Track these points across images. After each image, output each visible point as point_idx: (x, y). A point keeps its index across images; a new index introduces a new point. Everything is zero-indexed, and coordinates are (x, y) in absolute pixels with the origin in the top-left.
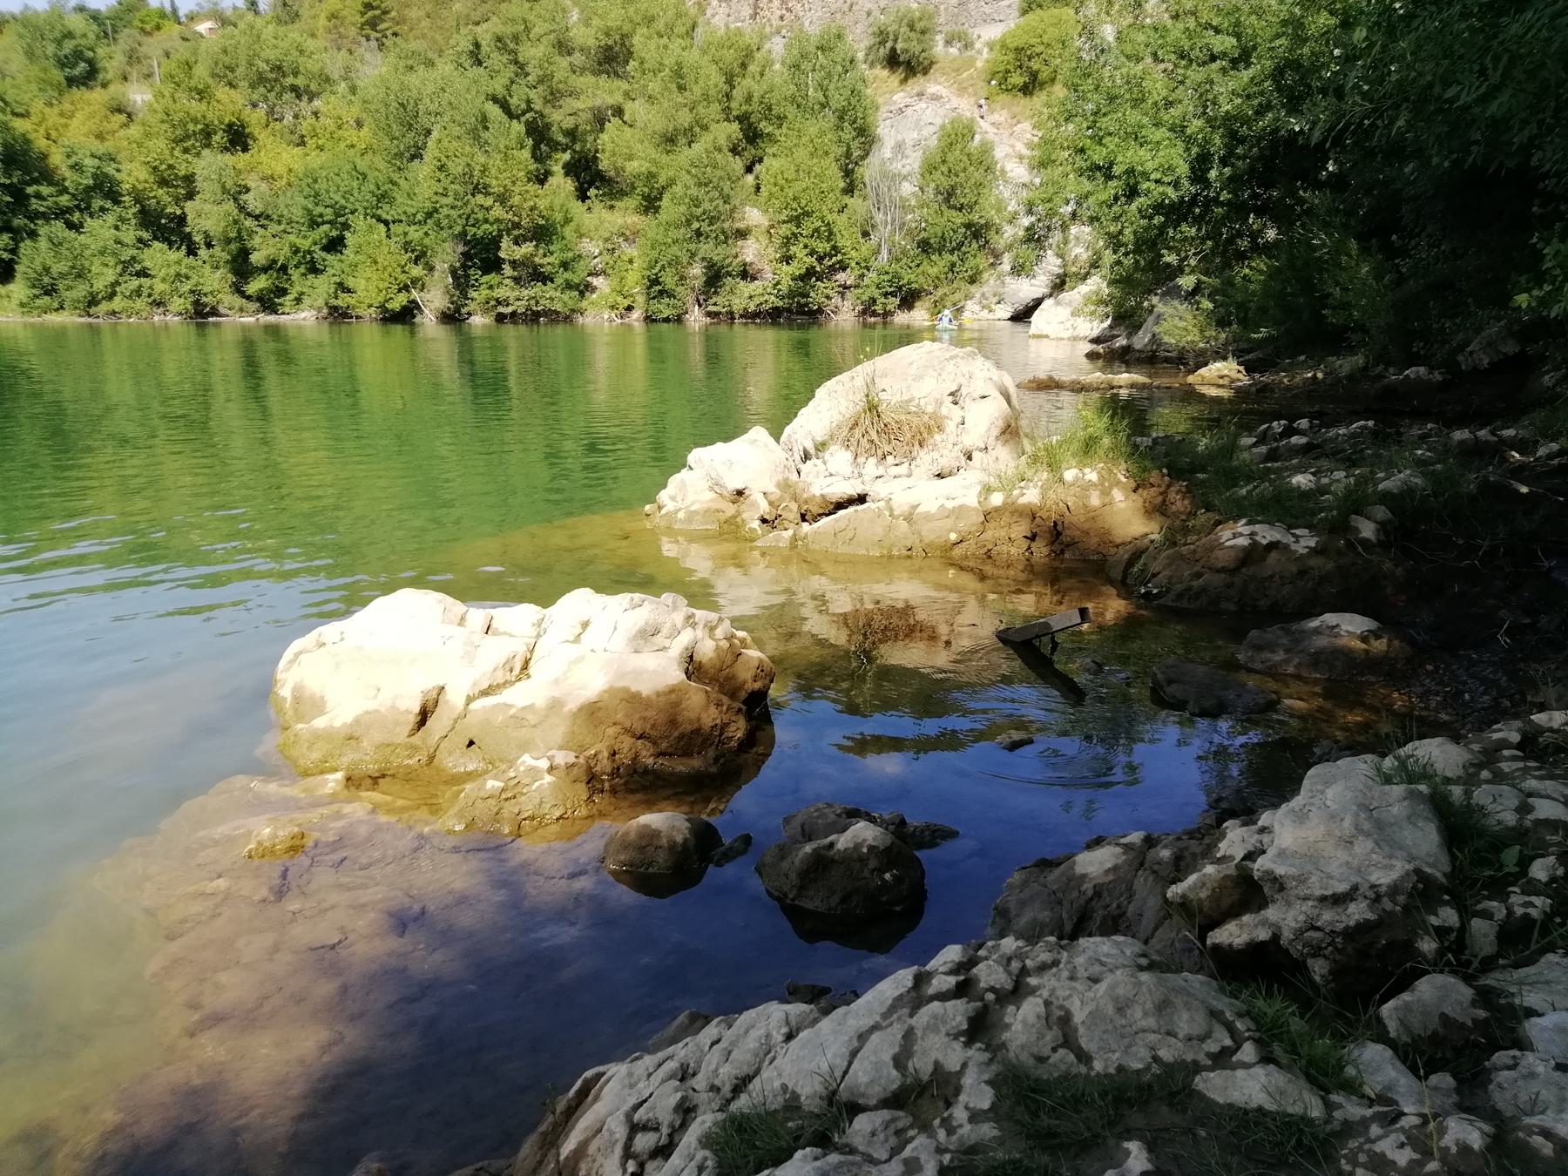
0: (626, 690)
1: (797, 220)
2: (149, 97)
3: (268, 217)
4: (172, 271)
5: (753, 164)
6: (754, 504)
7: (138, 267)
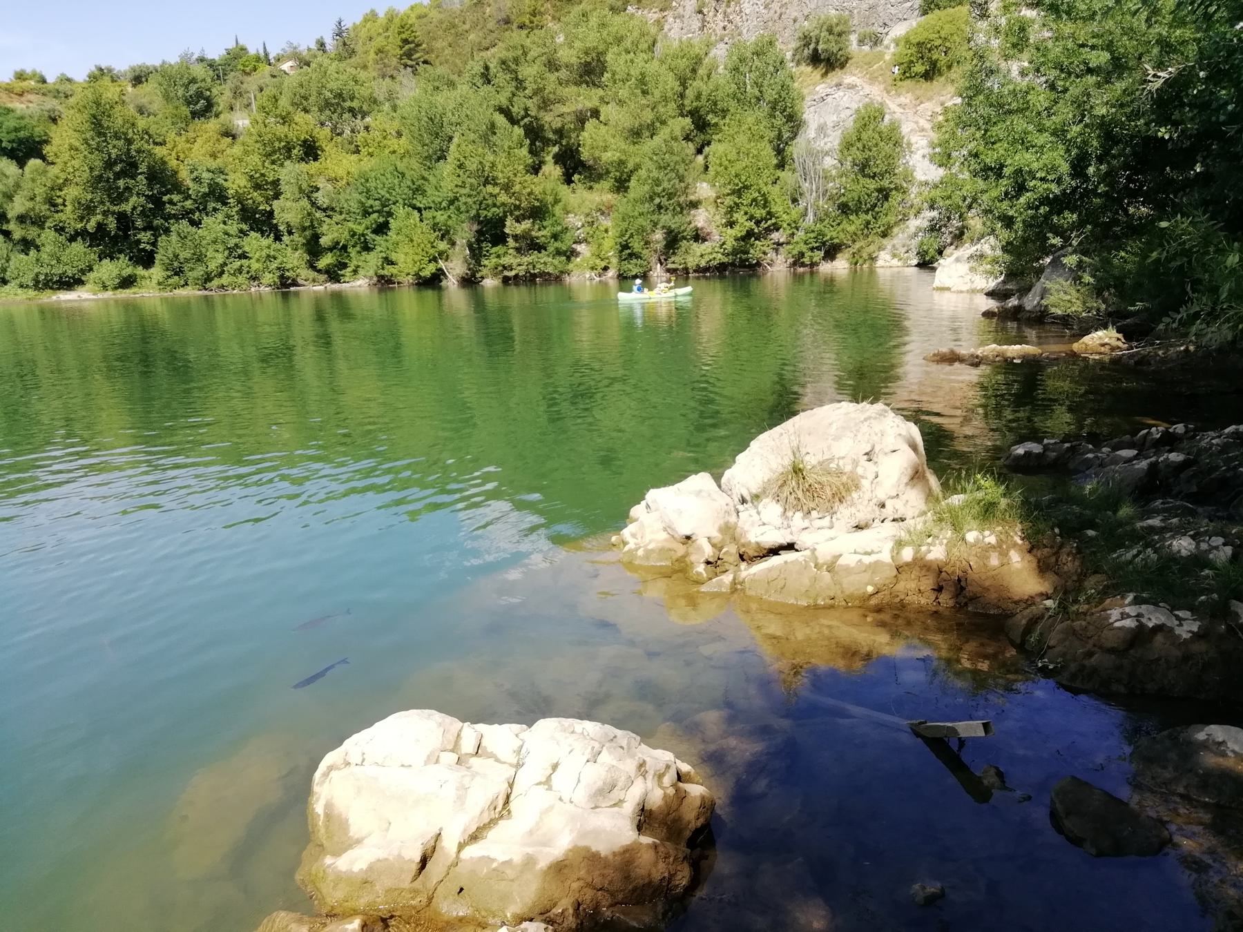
0: (587, 849)
1: (738, 193)
2: (247, 122)
3: (333, 209)
4: (264, 254)
5: (703, 146)
6: (700, 549)
7: (240, 251)
